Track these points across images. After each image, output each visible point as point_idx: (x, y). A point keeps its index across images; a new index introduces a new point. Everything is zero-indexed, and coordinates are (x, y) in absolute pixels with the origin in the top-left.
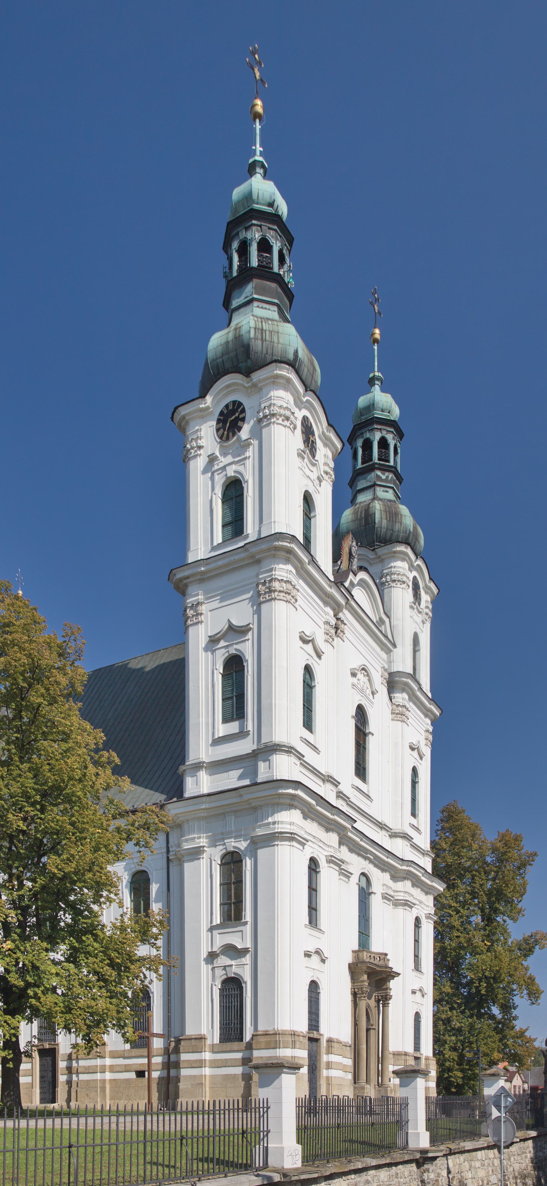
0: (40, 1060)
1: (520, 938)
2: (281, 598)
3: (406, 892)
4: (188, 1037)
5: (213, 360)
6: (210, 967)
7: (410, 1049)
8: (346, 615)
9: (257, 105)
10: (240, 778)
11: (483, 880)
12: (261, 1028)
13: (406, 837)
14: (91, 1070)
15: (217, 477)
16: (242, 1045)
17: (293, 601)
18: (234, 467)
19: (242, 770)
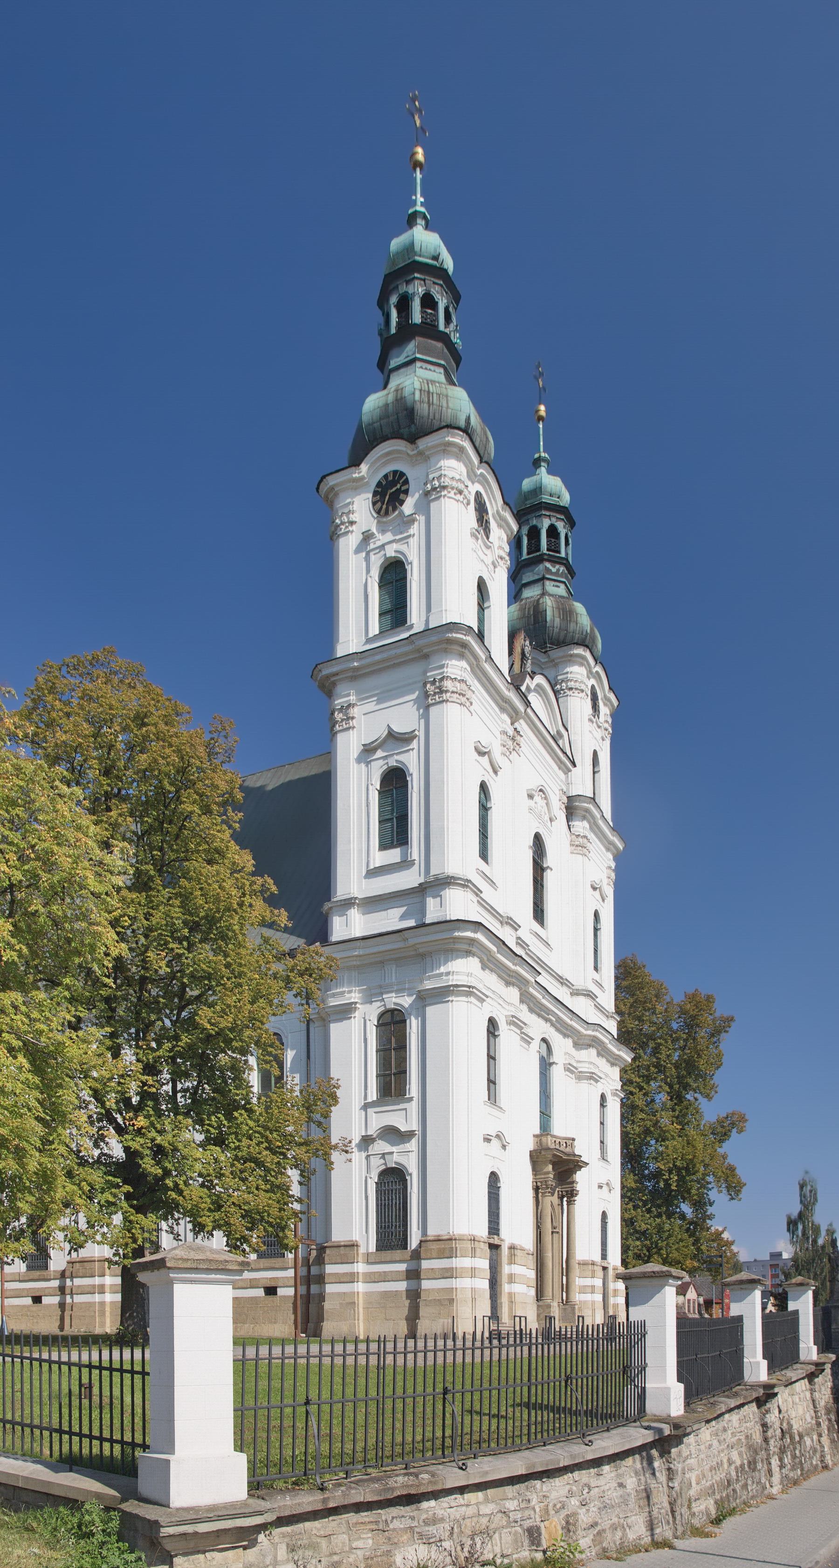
1: (713, 1119)
3: (591, 1063)
4: (335, 1244)
5: (369, 424)
6: (364, 1155)
7: (597, 1257)
10: (403, 917)
11: (669, 1049)
12: (432, 1232)
13: (590, 995)
15: (373, 557)
16: (407, 1254)
17: (468, 704)
18: (395, 546)
19: (405, 908)
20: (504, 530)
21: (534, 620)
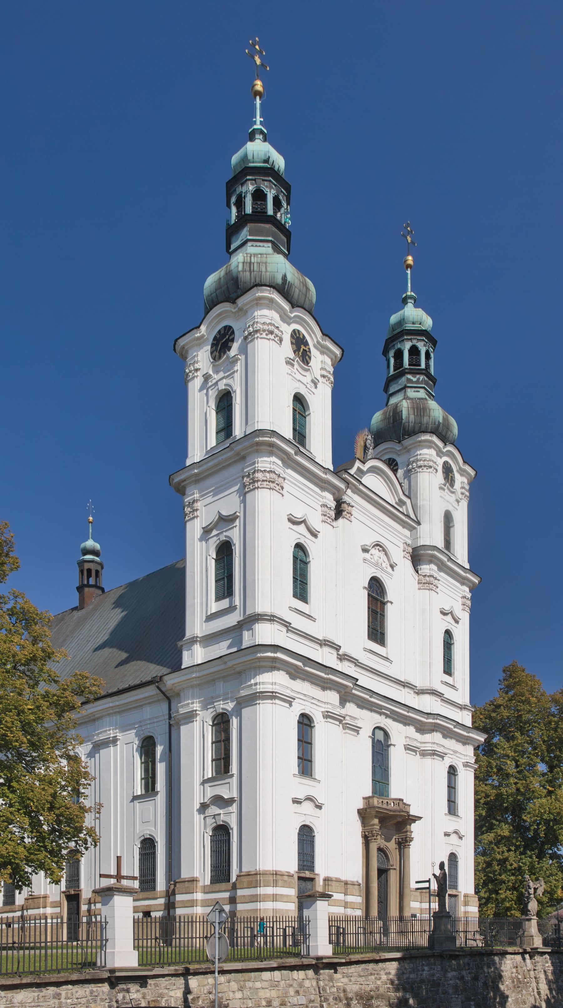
0: (68, 905)
2: (265, 486)
3: (434, 743)
4: (183, 880)
5: (209, 296)
6: (202, 816)
8: (350, 496)
10: (229, 647)
13: (433, 693)
15: (210, 392)
16: (229, 886)
18: (224, 381)
19: (231, 640)
21: (393, 420)
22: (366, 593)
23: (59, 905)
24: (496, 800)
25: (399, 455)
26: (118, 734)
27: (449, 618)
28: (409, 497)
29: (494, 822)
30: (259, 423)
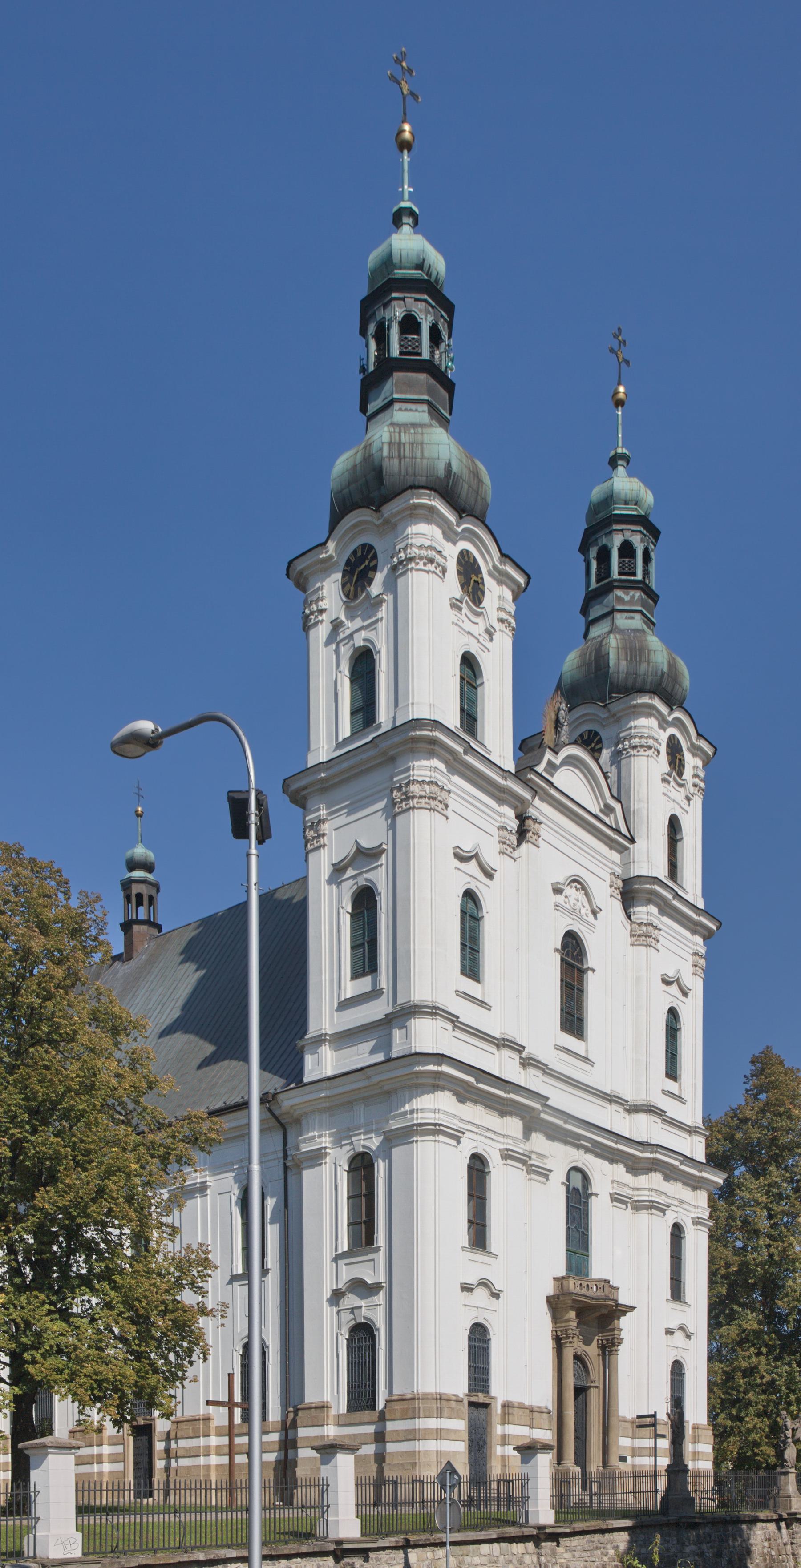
2: (423, 805)
3: (652, 1190)
4: (307, 1406)
6: (335, 1309)
8: (540, 809)
9: (404, 131)
10: (373, 1052)
12: (397, 1391)
13: (652, 1110)
14: (194, 1453)
15: (342, 649)
18: (363, 634)
20: (507, 586)
22: (558, 957)
23: (122, 1441)
24: (737, 1273)
25: (604, 726)
26: (208, 1179)
27: (674, 989)
28: (619, 800)
29: (735, 1307)
30: (415, 706)
